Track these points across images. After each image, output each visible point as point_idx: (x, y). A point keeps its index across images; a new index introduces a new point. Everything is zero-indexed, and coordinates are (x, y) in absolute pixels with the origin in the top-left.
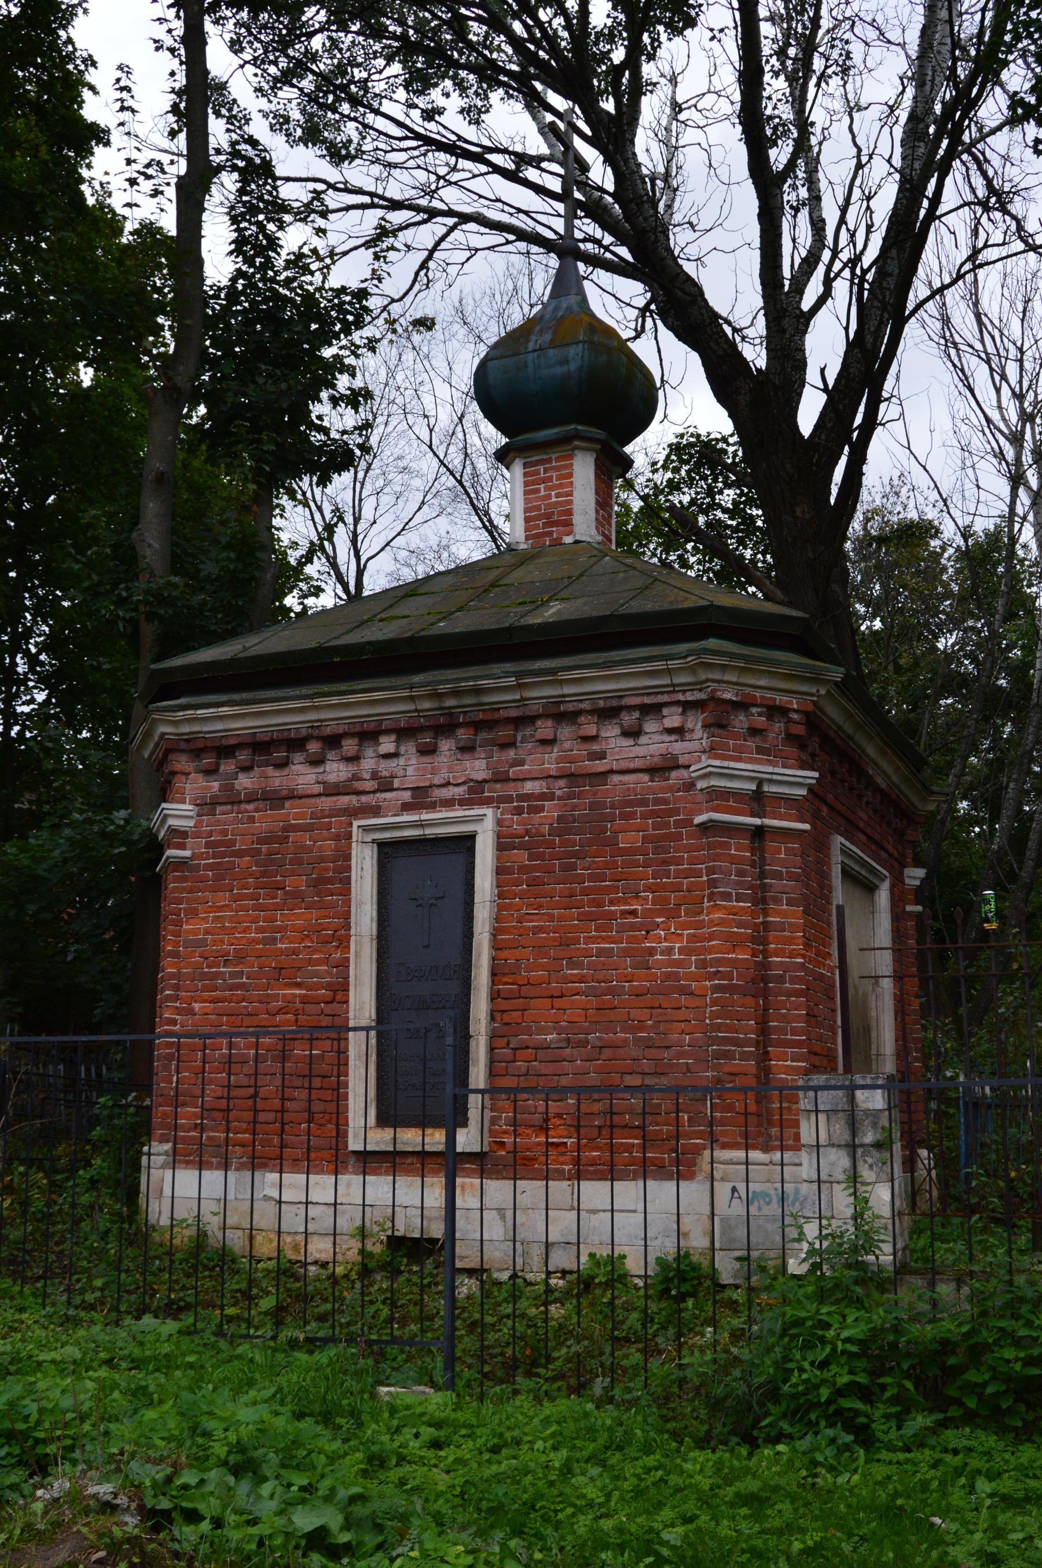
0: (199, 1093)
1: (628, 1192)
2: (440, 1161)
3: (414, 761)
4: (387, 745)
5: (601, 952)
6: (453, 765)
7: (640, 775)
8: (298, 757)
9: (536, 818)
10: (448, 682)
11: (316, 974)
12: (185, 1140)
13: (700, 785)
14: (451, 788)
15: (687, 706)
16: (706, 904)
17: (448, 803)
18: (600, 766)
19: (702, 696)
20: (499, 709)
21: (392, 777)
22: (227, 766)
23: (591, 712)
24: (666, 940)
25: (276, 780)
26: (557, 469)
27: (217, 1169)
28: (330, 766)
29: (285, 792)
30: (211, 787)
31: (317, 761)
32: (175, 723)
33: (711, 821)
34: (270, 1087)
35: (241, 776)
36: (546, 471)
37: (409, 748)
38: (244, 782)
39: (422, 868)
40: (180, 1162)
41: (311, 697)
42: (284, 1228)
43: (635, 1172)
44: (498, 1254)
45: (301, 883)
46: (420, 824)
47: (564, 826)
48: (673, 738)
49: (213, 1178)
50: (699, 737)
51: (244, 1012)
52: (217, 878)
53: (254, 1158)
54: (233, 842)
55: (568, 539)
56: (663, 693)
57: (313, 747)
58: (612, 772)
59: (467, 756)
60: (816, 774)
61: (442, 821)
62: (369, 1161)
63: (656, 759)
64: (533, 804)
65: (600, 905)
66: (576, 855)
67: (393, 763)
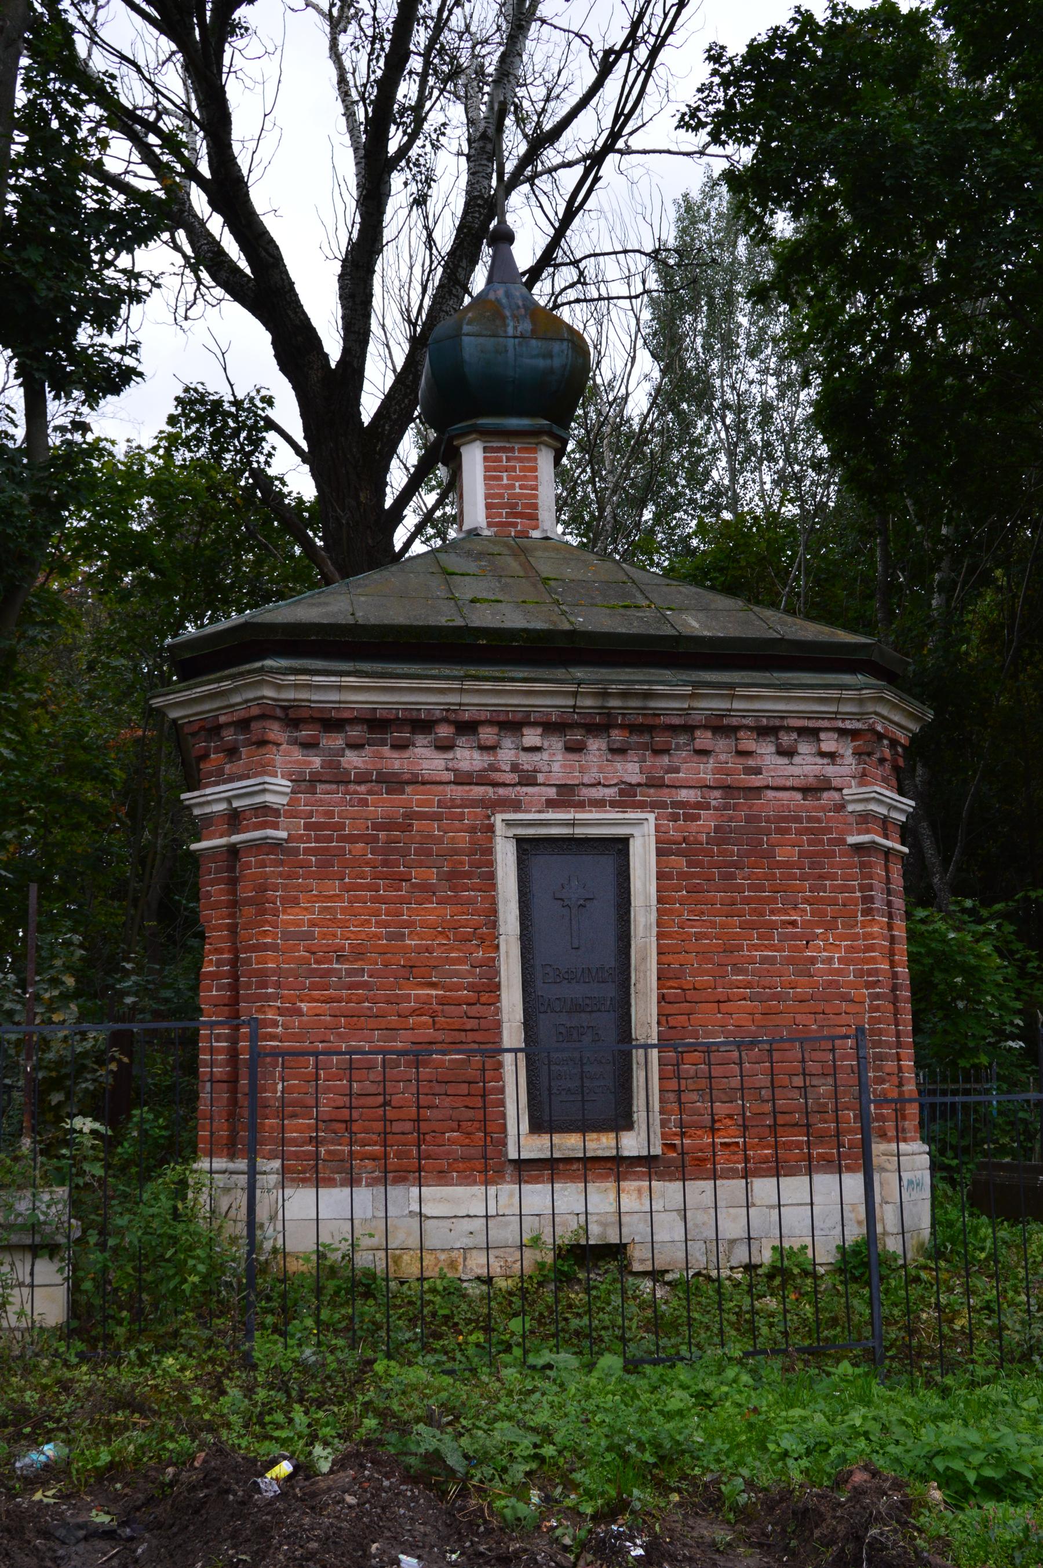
0: (313, 1103)
1: (794, 1187)
2: (609, 1165)
3: (559, 757)
4: (532, 737)
5: (764, 960)
6: (598, 764)
7: (794, 793)
8: (421, 739)
9: (694, 826)
10: (621, 682)
11: (456, 974)
12: (297, 1156)
13: (850, 808)
14: (600, 788)
15: (842, 732)
16: (860, 918)
17: (599, 804)
18: (756, 781)
19: (859, 725)
20: (659, 715)
21: (535, 771)
22: (335, 741)
23: (706, 727)
24: (825, 950)
25: (396, 762)
26: (521, 460)
27: (342, 1185)
28: (459, 753)
29: (406, 777)
30: (310, 763)
31: (445, 747)
32: (279, 687)
33: (874, 842)
34: (404, 1095)
35: (348, 752)
36: (508, 459)
37: (556, 743)
38: (353, 760)
39: (576, 870)
40: (293, 1180)
41: (461, 679)
42: (427, 1244)
43: (769, 1169)
46: (573, 823)
47: (721, 836)
48: (825, 761)
49: (365, 1197)
50: (849, 764)
51: (369, 1013)
52: (320, 865)
53: (386, 1172)
54: (342, 826)
55: (536, 534)
56: (823, 719)
57: (444, 731)
58: (767, 787)
59: (618, 758)
60: (913, 803)
61: (596, 822)
62: (526, 1170)
63: (811, 779)
64: (689, 812)
65: (762, 914)
66: (735, 865)
67: (536, 757)
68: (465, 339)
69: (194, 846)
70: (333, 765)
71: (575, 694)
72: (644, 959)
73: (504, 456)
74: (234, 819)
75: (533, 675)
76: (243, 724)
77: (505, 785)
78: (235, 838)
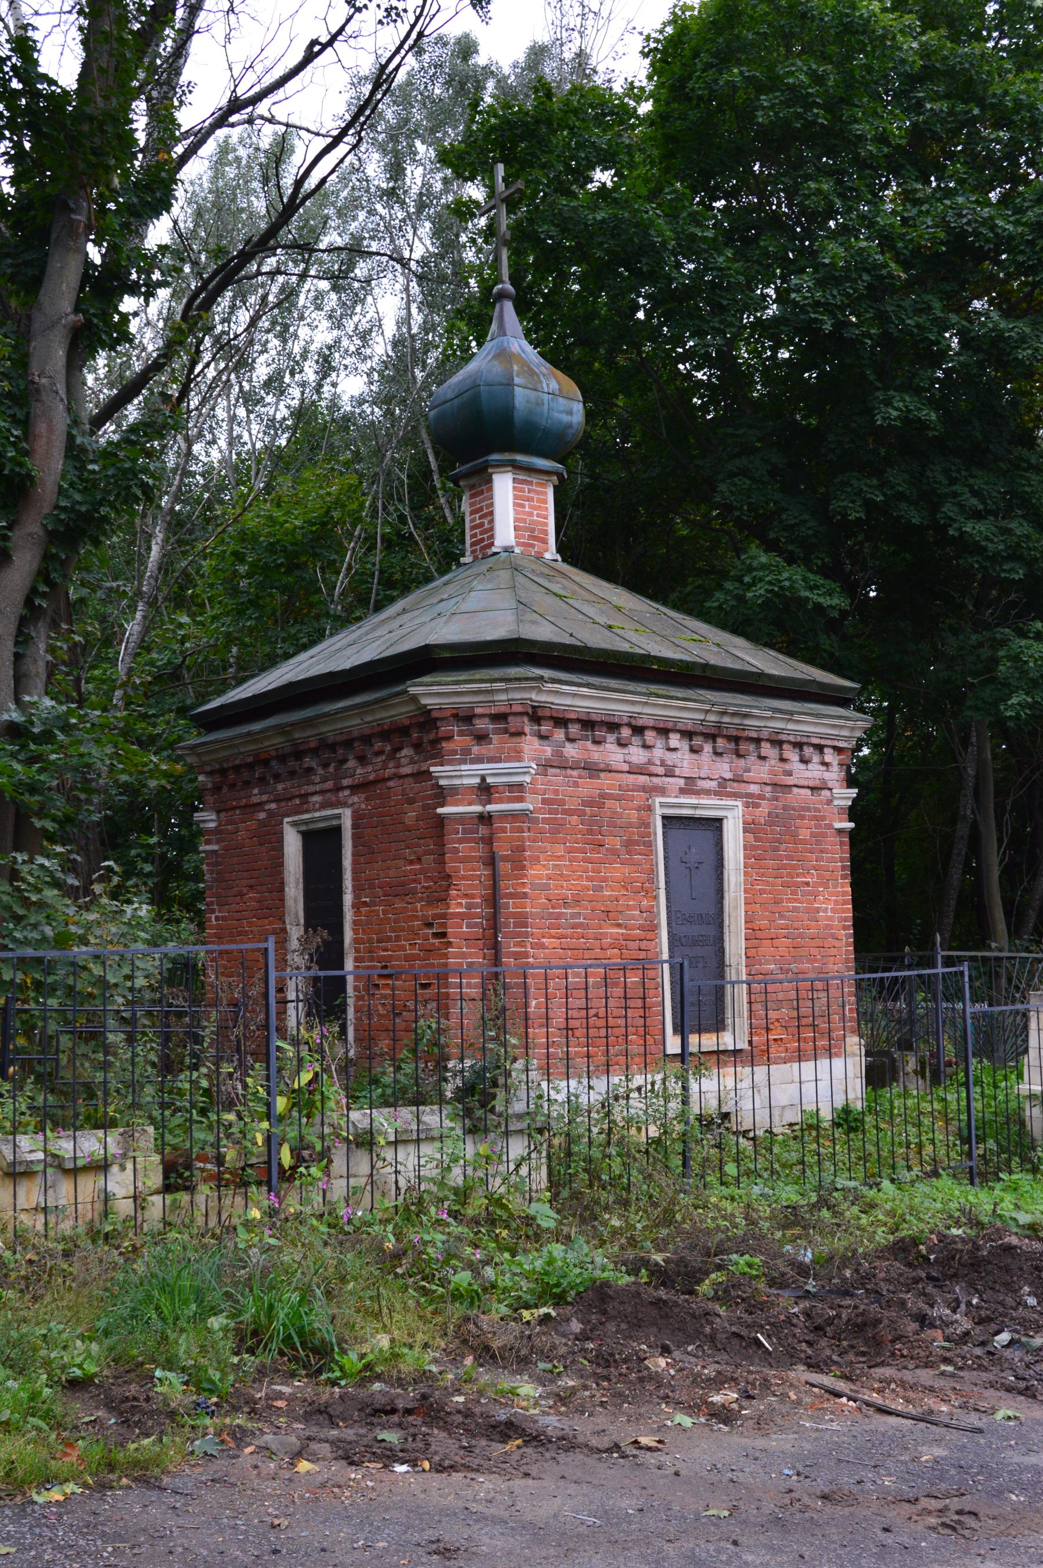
6: (712, 766)
10: (736, 705)
11: (633, 917)
13: (836, 803)
17: (707, 792)
18: (790, 780)
23: (767, 740)
25: (595, 754)
26: (538, 493)
29: (602, 766)
30: (545, 751)
35: (567, 744)
36: (529, 491)
38: (571, 751)
44: (762, 1119)
45: (616, 842)
46: (695, 807)
54: (562, 803)
61: (707, 806)
68: (517, 389)
69: (440, 810)
70: (558, 754)
71: (707, 712)
72: (736, 908)
73: (526, 487)
74: (485, 791)
75: (620, 687)
76: (499, 718)
77: (657, 775)
78: (490, 808)
